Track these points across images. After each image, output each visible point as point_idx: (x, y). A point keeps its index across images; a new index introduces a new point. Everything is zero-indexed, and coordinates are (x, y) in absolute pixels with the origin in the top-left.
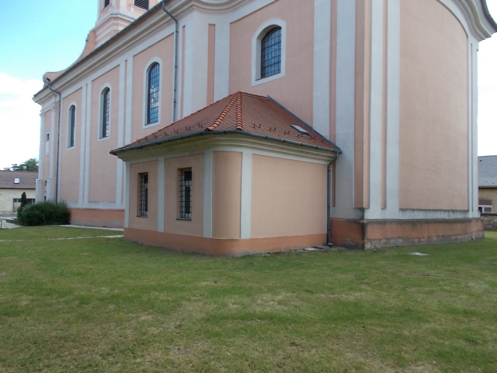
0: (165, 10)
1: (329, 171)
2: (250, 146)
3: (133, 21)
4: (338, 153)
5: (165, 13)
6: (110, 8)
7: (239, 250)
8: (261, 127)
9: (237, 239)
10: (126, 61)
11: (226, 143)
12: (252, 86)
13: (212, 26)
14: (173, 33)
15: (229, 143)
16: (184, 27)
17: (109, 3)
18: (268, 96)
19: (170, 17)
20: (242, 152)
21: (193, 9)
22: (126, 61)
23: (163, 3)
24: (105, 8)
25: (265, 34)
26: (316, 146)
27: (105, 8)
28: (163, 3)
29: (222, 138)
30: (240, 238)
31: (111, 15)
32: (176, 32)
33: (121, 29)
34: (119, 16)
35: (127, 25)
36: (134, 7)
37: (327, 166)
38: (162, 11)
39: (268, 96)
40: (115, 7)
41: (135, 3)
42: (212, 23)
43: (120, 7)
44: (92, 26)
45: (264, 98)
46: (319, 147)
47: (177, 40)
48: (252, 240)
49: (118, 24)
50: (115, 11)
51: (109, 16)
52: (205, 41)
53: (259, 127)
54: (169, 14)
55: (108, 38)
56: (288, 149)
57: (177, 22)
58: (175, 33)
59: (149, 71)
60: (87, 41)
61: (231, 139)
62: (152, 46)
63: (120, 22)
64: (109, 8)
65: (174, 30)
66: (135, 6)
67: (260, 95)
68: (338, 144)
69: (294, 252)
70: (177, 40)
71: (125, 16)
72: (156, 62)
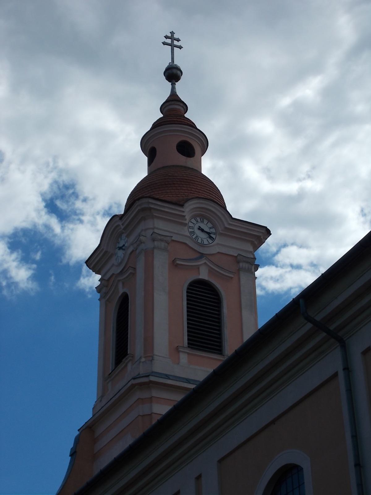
0: (309, 319)
3: (192, 386)
5: (309, 326)
6: (129, 365)
10: (199, 478)
14: (336, 375)
17: (127, 354)
19: (324, 334)
22: (199, 478)
23: (301, 301)
24: (116, 367)
27: (116, 367)
28: (301, 301)
31: (134, 378)
32: (344, 369)
33: (162, 409)
34: (152, 378)
35: (178, 397)
36: (188, 353)
40: (143, 360)
41: (188, 343)
43: (155, 357)
44: (87, 415)
47: (350, 390)
49: (151, 400)
50: (142, 370)
51: (130, 384)
54: (320, 326)
55: (128, 441)
58: (341, 375)
60: (73, 454)
62: (273, 422)
63: (155, 393)
64: (126, 366)
65: (339, 366)
66: (189, 349)
70: (350, 390)
71: (167, 377)
72: (290, 464)
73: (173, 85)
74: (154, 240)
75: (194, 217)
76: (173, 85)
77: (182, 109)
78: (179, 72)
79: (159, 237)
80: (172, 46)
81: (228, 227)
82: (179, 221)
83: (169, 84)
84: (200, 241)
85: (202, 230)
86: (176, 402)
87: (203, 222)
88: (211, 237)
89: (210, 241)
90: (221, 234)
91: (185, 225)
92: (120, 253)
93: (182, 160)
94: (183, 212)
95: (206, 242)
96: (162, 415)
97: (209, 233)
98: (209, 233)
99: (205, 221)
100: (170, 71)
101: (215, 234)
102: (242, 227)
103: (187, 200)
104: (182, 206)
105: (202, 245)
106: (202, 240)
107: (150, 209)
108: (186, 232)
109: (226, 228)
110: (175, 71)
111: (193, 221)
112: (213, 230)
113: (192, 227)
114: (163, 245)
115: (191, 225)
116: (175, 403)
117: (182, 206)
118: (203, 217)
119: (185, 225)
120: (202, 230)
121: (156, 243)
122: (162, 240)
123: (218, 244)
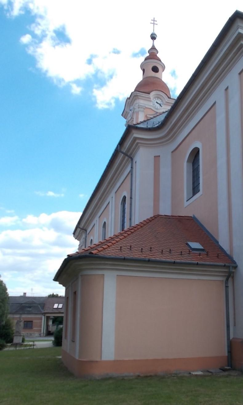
1: (227, 287)
2: (217, 275)
4: (231, 267)
7: (98, 372)
8: (152, 250)
9: (98, 360)
11: (93, 267)
12: (185, 207)
13: (157, 158)
15: (89, 267)
16: (136, 162)
18: (194, 215)
20: (104, 275)
21: (139, 147)
25: (194, 157)
26: (196, 262)
29: (81, 263)
30: (101, 359)
37: (224, 282)
38: (120, 153)
39: (194, 215)
42: (157, 155)
45: (183, 218)
46: (199, 262)
48: (115, 363)
52: (151, 172)
53: (150, 249)
56: (162, 268)
57: (132, 159)
59: (123, 204)
61: (88, 262)
67: (183, 216)
68: (235, 259)
69: (26, 313)
73: (153, 41)
74: (139, 108)
75: (155, 98)
76: (153, 41)
77: (156, 52)
78: (155, 36)
79: (141, 106)
80: (154, 24)
81: (167, 101)
82: (149, 100)
83: (152, 40)
84: (156, 107)
85: (158, 103)
86: (167, 113)
87: (158, 99)
88: (161, 106)
89: (161, 107)
90: (165, 104)
91: (151, 101)
92: (130, 112)
93: (153, 74)
94: (149, 96)
95: (159, 108)
96: (174, 99)
97: (160, 104)
98: (160, 104)
99: (159, 99)
100: (152, 36)
101: (162, 104)
102: (146, 97)
103: (152, 91)
104: (149, 94)
105: (157, 109)
106: (157, 107)
107: (137, 95)
108: (151, 104)
109: (167, 102)
110: (154, 36)
111: (154, 99)
112: (162, 103)
113: (154, 102)
114: (142, 109)
115: (153, 101)
116: (172, 105)
117: (149, 94)
118: (158, 98)
119: (151, 101)
120: (158, 103)
121: (140, 109)
122: (142, 108)
123: (163, 108)
